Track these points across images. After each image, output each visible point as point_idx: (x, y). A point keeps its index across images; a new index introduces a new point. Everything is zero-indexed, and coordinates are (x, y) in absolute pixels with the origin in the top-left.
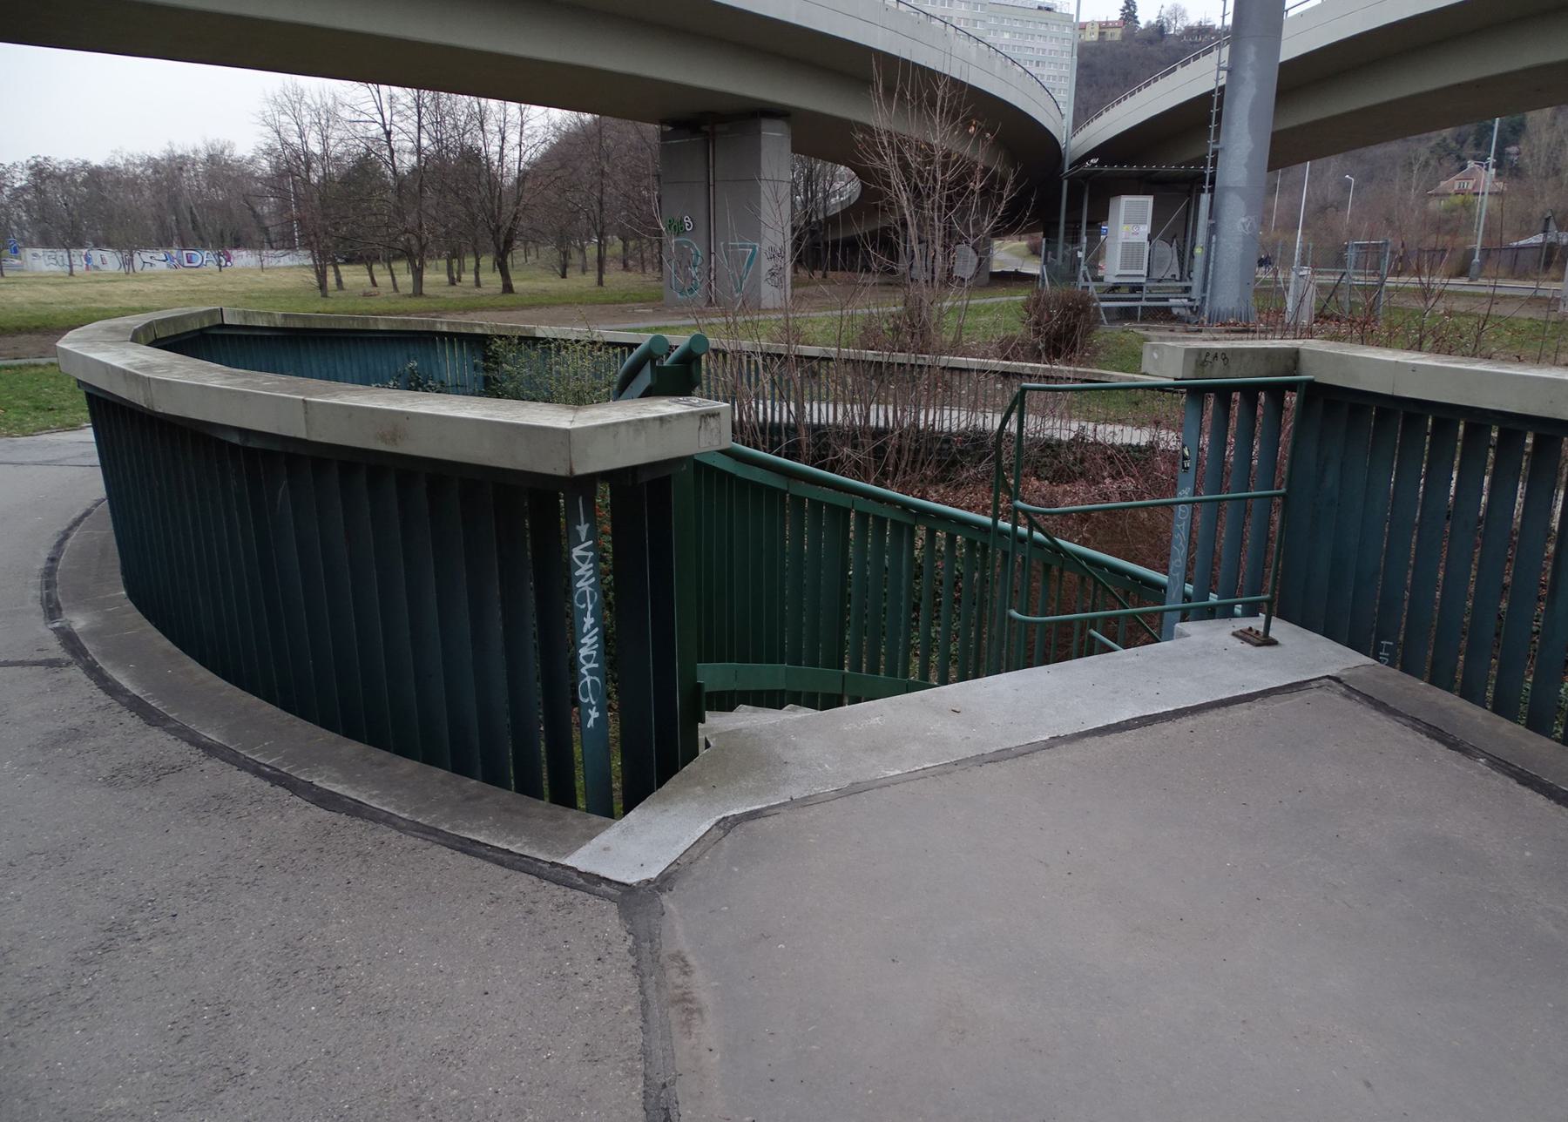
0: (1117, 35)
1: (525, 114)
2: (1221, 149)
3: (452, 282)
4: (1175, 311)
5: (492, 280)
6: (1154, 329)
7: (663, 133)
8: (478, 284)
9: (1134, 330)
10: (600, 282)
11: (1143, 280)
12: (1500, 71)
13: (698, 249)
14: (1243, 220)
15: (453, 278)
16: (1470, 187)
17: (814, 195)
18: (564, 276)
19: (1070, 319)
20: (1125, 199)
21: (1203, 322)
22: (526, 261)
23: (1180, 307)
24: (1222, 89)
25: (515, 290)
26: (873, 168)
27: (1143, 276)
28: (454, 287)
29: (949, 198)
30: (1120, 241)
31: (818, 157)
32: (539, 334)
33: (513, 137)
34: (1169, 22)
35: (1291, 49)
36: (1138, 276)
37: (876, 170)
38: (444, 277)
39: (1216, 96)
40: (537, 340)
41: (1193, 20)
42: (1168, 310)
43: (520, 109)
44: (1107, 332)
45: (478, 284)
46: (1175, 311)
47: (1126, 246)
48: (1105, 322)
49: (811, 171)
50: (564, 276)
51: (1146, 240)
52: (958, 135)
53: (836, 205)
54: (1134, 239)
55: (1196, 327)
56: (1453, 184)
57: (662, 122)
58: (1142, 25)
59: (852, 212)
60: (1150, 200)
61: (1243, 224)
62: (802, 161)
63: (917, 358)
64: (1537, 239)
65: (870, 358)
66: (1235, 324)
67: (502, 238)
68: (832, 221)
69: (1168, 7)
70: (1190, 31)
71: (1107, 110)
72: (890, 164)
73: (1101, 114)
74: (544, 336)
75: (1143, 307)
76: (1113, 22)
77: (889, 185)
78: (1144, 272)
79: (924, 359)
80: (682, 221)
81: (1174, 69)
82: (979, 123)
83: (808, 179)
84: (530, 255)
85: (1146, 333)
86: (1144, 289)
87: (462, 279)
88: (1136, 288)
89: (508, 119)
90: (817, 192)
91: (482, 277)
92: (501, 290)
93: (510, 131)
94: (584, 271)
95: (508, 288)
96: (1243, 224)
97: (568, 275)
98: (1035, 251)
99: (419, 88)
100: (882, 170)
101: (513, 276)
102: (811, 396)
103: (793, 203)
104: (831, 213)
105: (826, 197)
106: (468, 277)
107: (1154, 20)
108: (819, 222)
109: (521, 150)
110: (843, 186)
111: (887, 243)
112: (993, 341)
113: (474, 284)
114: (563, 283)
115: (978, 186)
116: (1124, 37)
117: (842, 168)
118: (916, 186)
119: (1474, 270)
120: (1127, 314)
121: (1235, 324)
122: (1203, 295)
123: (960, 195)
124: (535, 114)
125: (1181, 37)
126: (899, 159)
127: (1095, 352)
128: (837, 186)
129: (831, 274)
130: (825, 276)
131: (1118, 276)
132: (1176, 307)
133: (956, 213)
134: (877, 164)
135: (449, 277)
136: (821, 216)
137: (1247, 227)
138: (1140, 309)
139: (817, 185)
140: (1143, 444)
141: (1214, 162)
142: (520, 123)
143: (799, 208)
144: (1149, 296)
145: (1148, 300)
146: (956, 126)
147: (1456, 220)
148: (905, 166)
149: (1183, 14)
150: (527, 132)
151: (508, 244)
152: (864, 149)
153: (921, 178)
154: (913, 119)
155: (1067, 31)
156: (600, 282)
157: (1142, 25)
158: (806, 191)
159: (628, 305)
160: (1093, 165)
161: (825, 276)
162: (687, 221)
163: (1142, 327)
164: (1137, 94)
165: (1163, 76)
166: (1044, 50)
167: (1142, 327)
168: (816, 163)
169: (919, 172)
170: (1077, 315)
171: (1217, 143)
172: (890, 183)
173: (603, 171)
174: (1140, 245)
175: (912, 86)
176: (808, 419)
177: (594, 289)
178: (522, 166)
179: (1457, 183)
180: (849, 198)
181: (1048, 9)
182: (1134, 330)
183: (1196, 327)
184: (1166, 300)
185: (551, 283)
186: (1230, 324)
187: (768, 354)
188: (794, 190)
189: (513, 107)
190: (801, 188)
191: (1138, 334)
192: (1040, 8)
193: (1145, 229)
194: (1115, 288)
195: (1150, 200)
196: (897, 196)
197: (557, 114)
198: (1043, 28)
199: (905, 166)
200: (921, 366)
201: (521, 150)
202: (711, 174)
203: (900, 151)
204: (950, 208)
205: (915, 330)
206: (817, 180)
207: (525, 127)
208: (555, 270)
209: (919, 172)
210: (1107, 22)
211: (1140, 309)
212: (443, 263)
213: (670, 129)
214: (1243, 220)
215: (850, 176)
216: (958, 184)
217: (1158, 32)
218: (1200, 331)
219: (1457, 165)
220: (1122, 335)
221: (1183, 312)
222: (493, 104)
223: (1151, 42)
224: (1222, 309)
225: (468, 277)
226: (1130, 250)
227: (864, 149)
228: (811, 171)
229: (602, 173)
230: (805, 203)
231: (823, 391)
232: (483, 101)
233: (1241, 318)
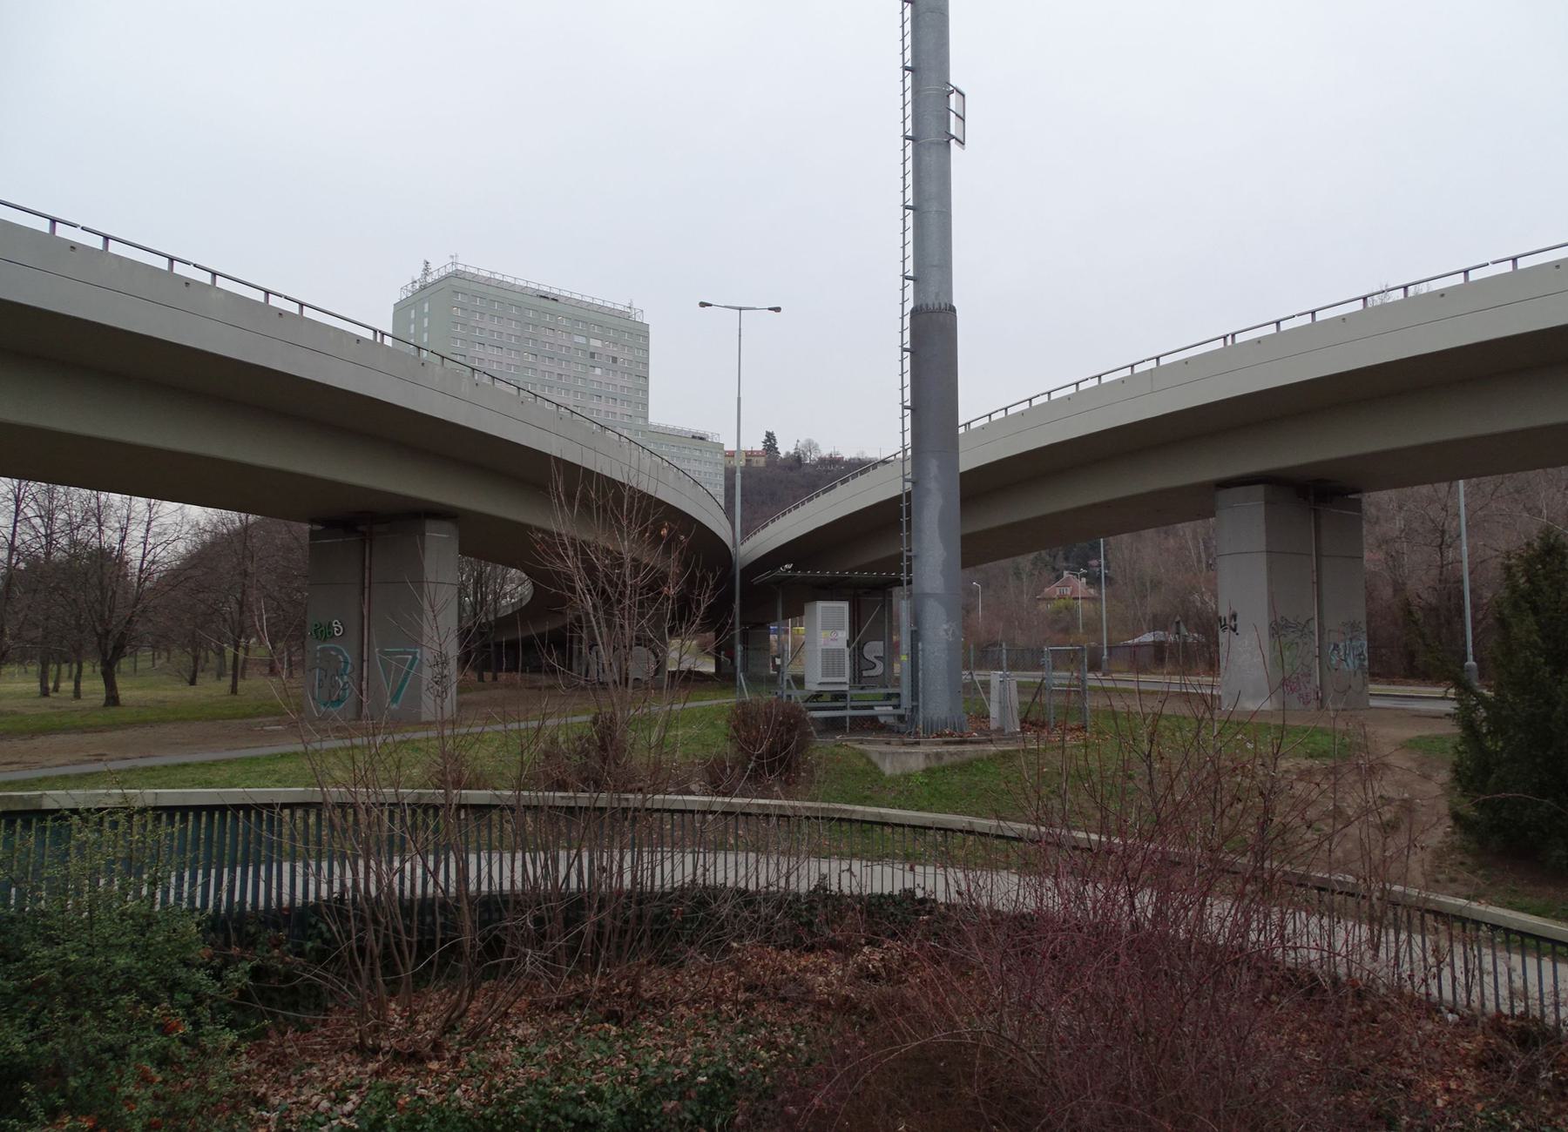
0: (762, 462)
1: (154, 511)
2: (915, 556)
3: (45, 692)
4: (882, 720)
5: (94, 686)
6: (869, 742)
7: (312, 533)
8: (77, 694)
9: (848, 743)
10: (234, 690)
11: (846, 688)
12: (1129, 493)
13: (349, 655)
14: (945, 627)
15: (47, 688)
16: (1069, 593)
17: (484, 599)
18: (192, 682)
19: (782, 735)
20: (820, 605)
21: (917, 733)
22: (154, 665)
23: (886, 715)
24: (909, 494)
25: (121, 702)
26: (554, 572)
27: (845, 683)
28: (46, 700)
29: (641, 604)
30: (819, 648)
31: (487, 559)
32: (48, 804)
33: (136, 533)
34: (805, 454)
35: (967, 462)
36: (841, 683)
37: (558, 573)
38: (35, 686)
39: (904, 505)
40: (42, 814)
41: (825, 452)
42: (874, 719)
43: (149, 505)
44: (823, 747)
45: (77, 694)
46: (882, 720)
47: (826, 652)
48: (815, 734)
49: (480, 574)
50: (192, 682)
51: (846, 647)
52: (649, 537)
53: (507, 606)
54: (834, 645)
55: (912, 739)
56: (1054, 590)
57: (312, 521)
58: (782, 455)
59: (525, 613)
60: (845, 605)
61: (946, 630)
62: (471, 563)
63: (619, 800)
64: (1148, 638)
65: (559, 803)
66: (951, 735)
67: (111, 645)
68: (507, 622)
69: (802, 441)
70: (822, 461)
71: (773, 521)
72: (572, 565)
73: (767, 525)
74: (56, 807)
75: (851, 717)
76: (758, 452)
77: (573, 590)
78: (846, 679)
79: (627, 800)
80: (330, 624)
81: (834, 487)
82: (672, 525)
83: (478, 582)
84: (159, 658)
85: (861, 747)
86: (848, 698)
87: (60, 689)
88: (839, 696)
89: (133, 515)
90: (487, 595)
91: (84, 686)
92: (103, 702)
93: (133, 527)
94: (220, 675)
95: (112, 699)
96: (946, 630)
97: (198, 681)
98: (703, 648)
99: (21, 477)
100: (564, 573)
101: (120, 683)
102: (479, 844)
103: (461, 605)
104: (501, 614)
105: (496, 600)
106: (67, 686)
107: (792, 452)
108: (489, 623)
109: (145, 549)
110: (515, 588)
111: (562, 642)
112: (697, 761)
113: (71, 695)
114: (190, 692)
115: (672, 592)
116: (768, 464)
117: (514, 571)
118: (604, 591)
119: (1105, 666)
120: (834, 725)
121: (951, 735)
122: (915, 704)
123: (654, 600)
124: (167, 511)
125: (815, 466)
126: (583, 562)
127: (811, 772)
128: (508, 588)
129: (503, 676)
130: (495, 678)
131: (820, 684)
132: (882, 715)
133: (649, 620)
134: (559, 566)
135: (41, 685)
136: (491, 618)
137: (950, 633)
138: (848, 719)
139: (487, 588)
140: (896, 892)
141: (909, 571)
142: (146, 519)
143: (468, 609)
144: (853, 704)
145: (853, 708)
146: (646, 529)
147: (1064, 622)
148: (590, 570)
149: (816, 447)
150: (154, 529)
151: (119, 651)
152: (544, 550)
153: (610, 582)
154: (598, 520)
155: (719, 456)
156: (234, 690)
157: (782, 455)
158: (475, 594)
159: (260, 720)
160: (787, 570)
161: (495, 678)
162: (336, 625)
163: (856, 740)
164: (801, 507)
165: (825, 492)
166: (700, 472)
167: (856, 740)
168: (486, 566)
169: (606, 575)
170: (789, 731)
171: (910, 550)
172: (575, 587)
173: (245, 571)
174: (840, 651)
175: (597, 485)
176: (472, 887)
177: (225, 698)
178: (145, 566)
179: (1058, 589)
180: (521, 600)
181: (701, 439)
182: (848, 743)
183: (912, 739)
184: (871, 708)
185: (175, 692)
186: (946, 735)
187: (419, 806)
188: (462, 590)
189: (140, 503)
190: (470, 589)
191: (854, 749)
192: (694, 437)
193: (844, 635)
194: (818, 696)
195: (845, 605)
196: (582, 601)
197: (196, 513)
198: (697, 453)
199: (590, 570)
200: (625, 810)
201: (145, 549)
202: (367, 575)
203: (584, 553)
204: (642, 616)
205: (606, 741)
206: (487, 583)
207: (153, 523)
208: (182, 676)
209: (606, 575)
210: (752, 452)
211: (848, 719)
212: (34, 668)
213: (320, 527)
214: (945, 627)
215: (520, 578)
216: (651, 589)
217: (796, 461)
218: (918, 743)
219: (1054, 575)
220: (836, 749)
221: (891, 720)
222: (116, 498)
223: (791, 469)
224: (935, 718)
225: (67, 686)
226: (830, 656)
227: (544, 550)
228: (480, 574)
229: (245, 574)
230: (474, 605)
231: (496, 833)
232: (103, 496)
233: (955, 728)
